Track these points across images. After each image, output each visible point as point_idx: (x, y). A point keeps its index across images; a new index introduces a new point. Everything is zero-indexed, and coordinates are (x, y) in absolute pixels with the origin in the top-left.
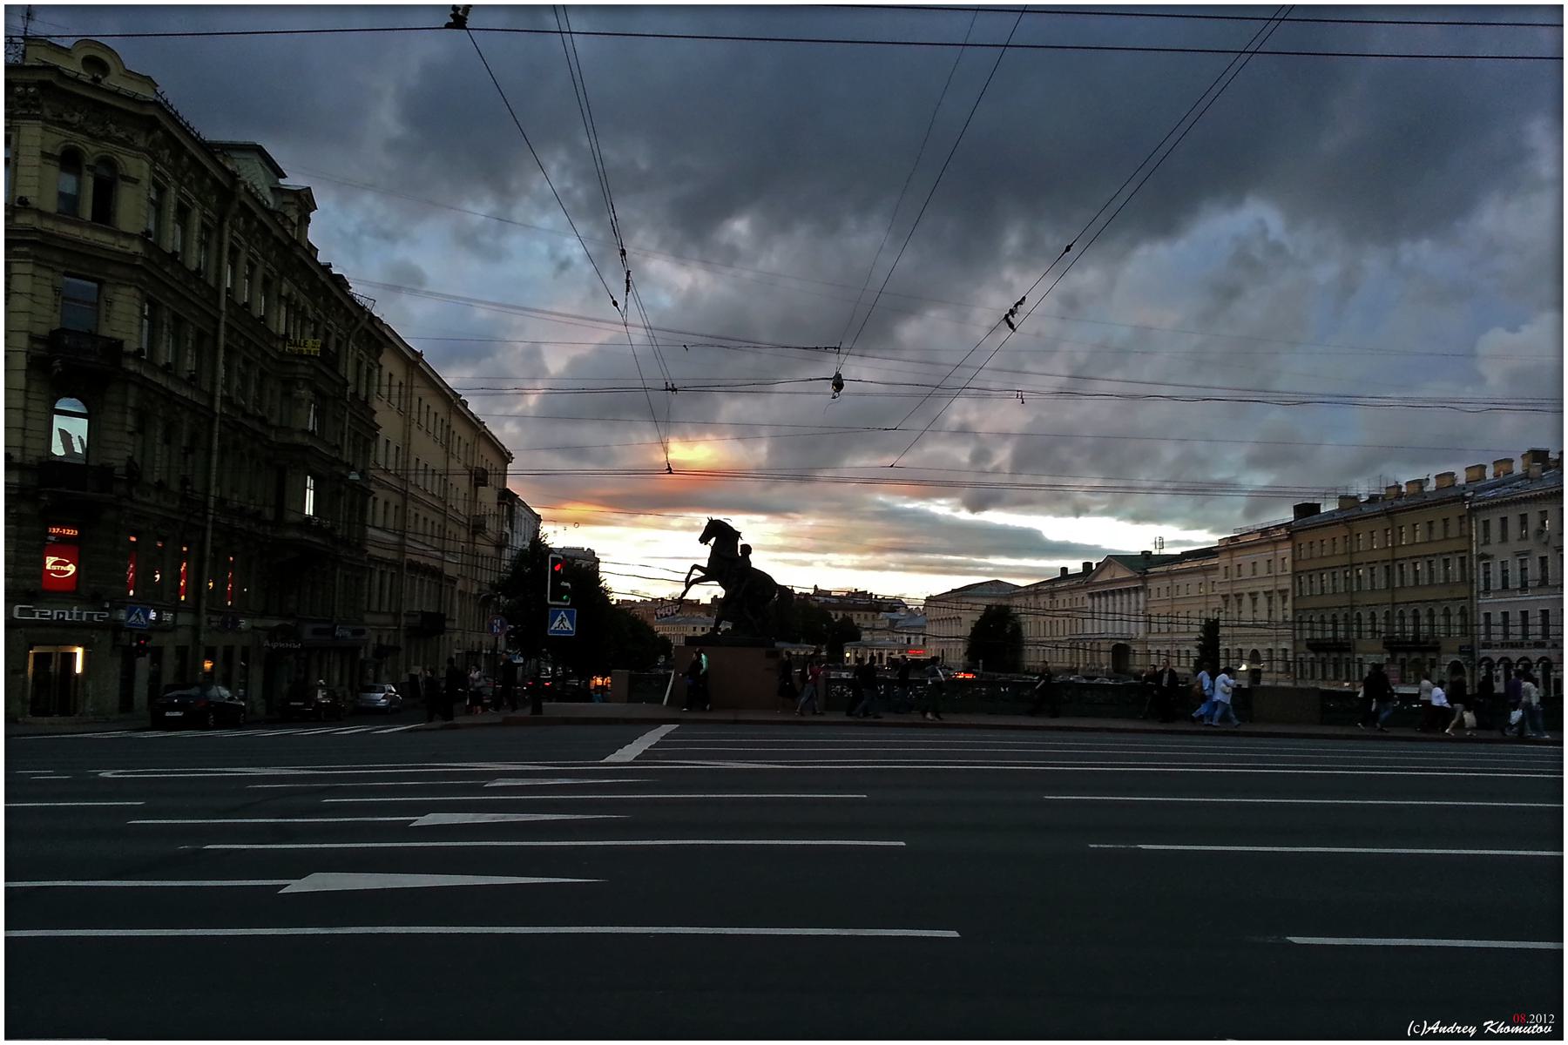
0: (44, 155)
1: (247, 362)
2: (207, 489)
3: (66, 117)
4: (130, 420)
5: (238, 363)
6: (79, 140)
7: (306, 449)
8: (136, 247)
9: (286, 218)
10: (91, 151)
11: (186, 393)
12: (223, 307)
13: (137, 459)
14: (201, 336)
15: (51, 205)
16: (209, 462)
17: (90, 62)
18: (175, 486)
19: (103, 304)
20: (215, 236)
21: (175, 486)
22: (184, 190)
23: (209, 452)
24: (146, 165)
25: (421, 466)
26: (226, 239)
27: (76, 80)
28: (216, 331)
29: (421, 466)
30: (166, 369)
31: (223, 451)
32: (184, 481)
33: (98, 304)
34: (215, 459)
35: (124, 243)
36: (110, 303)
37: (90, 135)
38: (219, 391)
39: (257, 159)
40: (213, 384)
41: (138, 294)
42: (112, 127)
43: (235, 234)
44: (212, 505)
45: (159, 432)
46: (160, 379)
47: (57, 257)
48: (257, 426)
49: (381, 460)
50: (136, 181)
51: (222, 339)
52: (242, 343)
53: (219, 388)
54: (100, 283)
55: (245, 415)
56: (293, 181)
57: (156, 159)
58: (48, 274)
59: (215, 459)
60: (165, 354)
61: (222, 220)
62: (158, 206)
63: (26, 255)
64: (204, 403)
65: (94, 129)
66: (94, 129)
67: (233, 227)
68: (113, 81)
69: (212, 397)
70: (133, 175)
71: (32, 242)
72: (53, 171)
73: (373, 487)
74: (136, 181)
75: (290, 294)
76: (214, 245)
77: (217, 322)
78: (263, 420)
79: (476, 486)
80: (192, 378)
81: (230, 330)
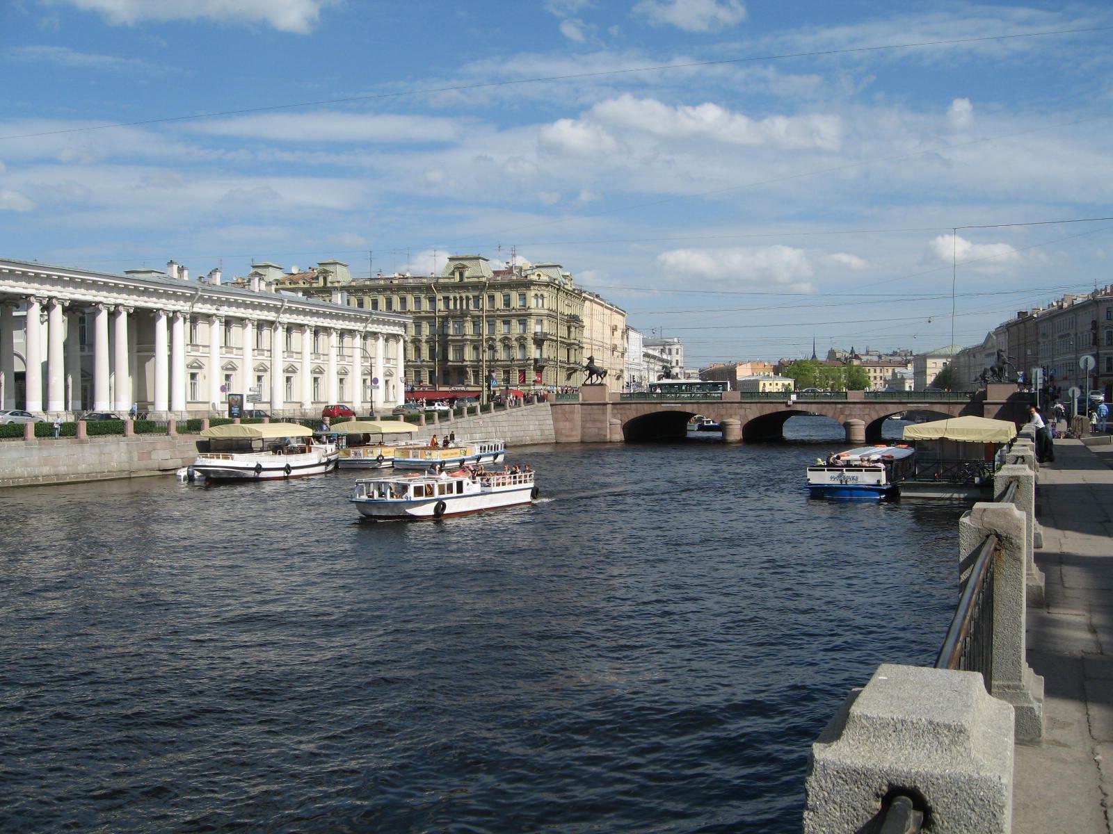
10: (539, 294)
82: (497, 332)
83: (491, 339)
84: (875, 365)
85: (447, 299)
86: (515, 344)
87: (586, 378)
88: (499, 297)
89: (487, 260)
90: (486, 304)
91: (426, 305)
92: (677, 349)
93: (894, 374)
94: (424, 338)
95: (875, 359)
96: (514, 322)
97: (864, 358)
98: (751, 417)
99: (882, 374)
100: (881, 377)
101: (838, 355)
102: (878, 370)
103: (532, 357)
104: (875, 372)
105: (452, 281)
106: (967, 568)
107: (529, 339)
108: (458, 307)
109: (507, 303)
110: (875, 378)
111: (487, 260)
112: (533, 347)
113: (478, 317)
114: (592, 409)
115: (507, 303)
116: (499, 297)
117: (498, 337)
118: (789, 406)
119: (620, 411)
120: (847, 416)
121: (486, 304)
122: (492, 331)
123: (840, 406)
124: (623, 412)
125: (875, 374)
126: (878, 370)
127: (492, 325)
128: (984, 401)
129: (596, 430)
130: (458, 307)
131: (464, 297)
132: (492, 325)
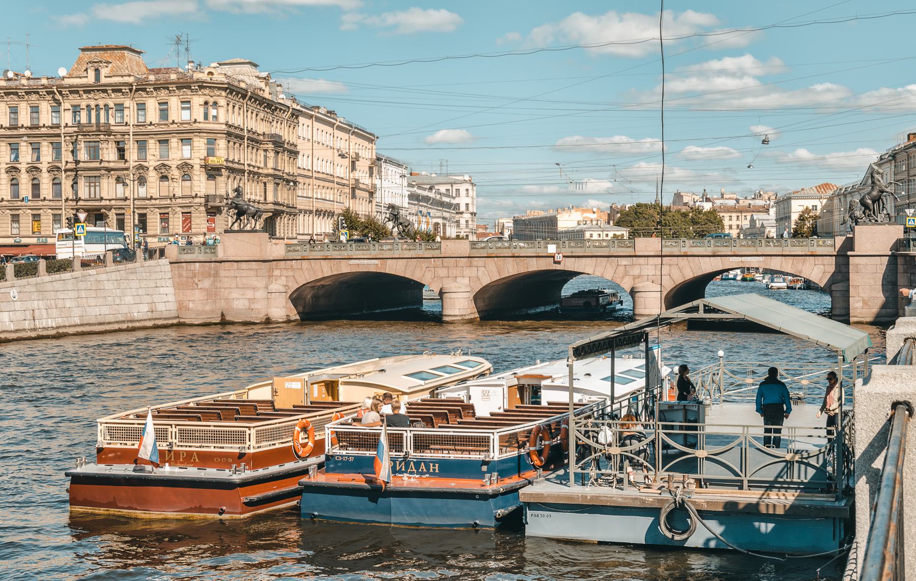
5: (250, 148)
10: (211, 100)
55: (254, 167)
66: (211, 94)
82: (149, 157)
83: (141, 167)
84: (729, 210)
85: (76, 110)
86: (176, 173)
87: (230, 220)
88: (152, 105)
89: (139, 53)
90: (131, 115)
91: (46, 117)
92: (467, 190)
93: (753, 221)
94: (44, 166)
95: (732, 203)
96: (174, 142)
97: (718, 202)
98: (486, 281)
99: (739, 223)
100: (738, 226)
101: (685, 200)
102: (734, 218)
103: (202, 194)
104: (730, 220)
105: (84, 81)
106: (878, 454)
107: (197, 167)
108: (93, 121)
109: (164, 113)
110: (731, 227)
111: (139, 53)
112: (203, 177)
113: (124, 134)
114: (210, 268)
115: (164, 113)
116: (152, 105)
117: (173, 164)
118: (559, 263)
119: (285, 273)
120: (635, 278)
121: (131, 115)
122: (165, 155)
123: (624, 261)
124: (290, 273)
125: (730, 223)
126: (734, 218)
127: (142, 146)
128: (849, 253)
129: (246, 303)
130: (93, 121)
131: (102, 106)
132: (142, 146)
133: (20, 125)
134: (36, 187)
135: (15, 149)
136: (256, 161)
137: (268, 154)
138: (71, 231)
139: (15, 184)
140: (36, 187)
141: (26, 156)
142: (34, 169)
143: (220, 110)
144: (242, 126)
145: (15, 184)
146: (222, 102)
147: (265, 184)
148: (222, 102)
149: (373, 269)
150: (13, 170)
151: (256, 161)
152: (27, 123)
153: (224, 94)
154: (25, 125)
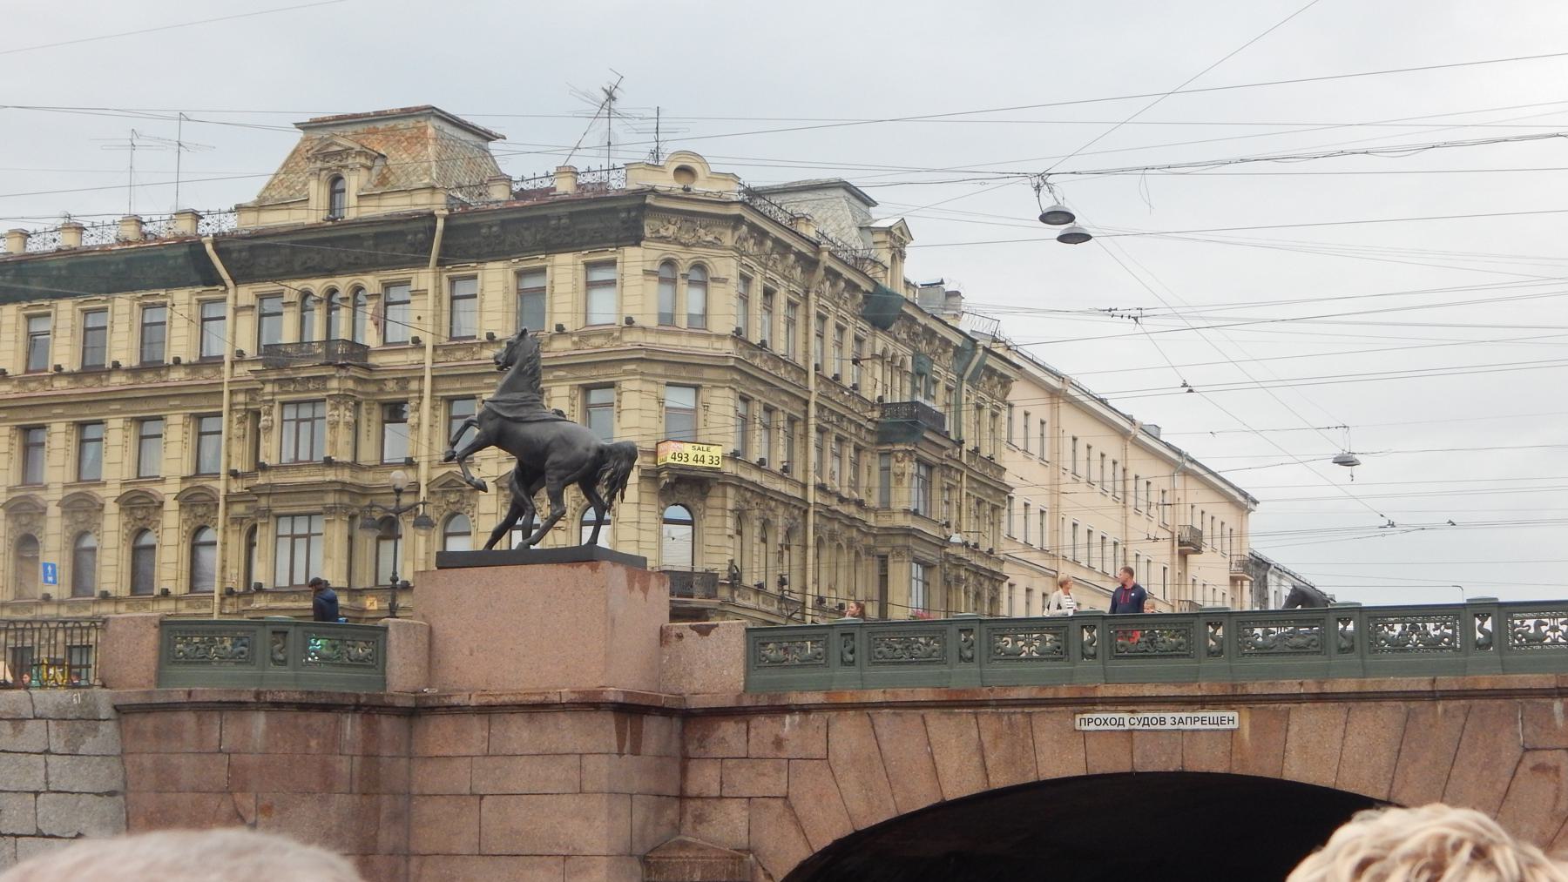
0: (647, 273)
1: (840, 440)
2: (805, 587)
3: (663, 233)
4: (730, 522)
5: (830, 444)
6: (673, 250)
7: (908, 532)
8: (728, 347)
9: (875, 263)
10: (685, 258)
11: (780, 486)
12: (812, 386)
13: (737, 563)
14: (792, 420)
15: (652, 322)
16: (805, 559)
17: (684, 171)
18: (772, 587)
19: (701, 412)
20: (801, 309)
21: (772, 587)
22: (769, 274)
23: (805, 547)
24: (733, 262)
25: (1096, 539)
26: (813, 310)
27: (667, 196)
28: (806, 413)
29: (1096, 539)
30: (760, 465)
31: (819, 543)
32: (782, 582)
33: (695, 410)
34: (811, 552)
35: (718, 345)
36: (706, 407)
37: (684, 245)
38: (812, 479)
39: (842, 192)
40: (806, 471)
41: (731, 394)
42: (702, 232)
43: (822, 301)
44: (809, 604)
45: (757, 531)
46: (755, 476)
47: (660, 369)
48: (851, 510)
49: (1018, 533)
50: (725, 281)
51: (812, 421)
52: (834, 419)
53: (811, 474)
54: (697, 388)
55: (842, 500)
56: (883, 217)
57: (742, 253)
58: (653, 387)
59: (811, 552)
60: (756, 453)
61: (807, 292)
62: (744, 299)
63: (633, 373)
64: (798, 493)
65: (686, 238)
66: (686, 238)
67: (818, 294)
68: (699, 187)
69: (805, 486)
70: (722, 275)
71: (642, 359)
72: (653, 285)
73: (1006, 569)
74: (725, 281)
75: (885, 351)
76: (800, 320)
77: (807, 403)
78: (860, 504)
79: (1183, 556)
80: (785, 469)
81: (821, 408)
108: (317, 334)
133: (169, 360)
134: (141, 555)
135: (30, 440)
136: (855, 485)
137: (896, 467)
138: (76, 697)
139: (27, 544)
140: (141, 555)
141: (57, 465)
142: (82, 507)
143: (716, 292)
144: (800, 361)
145: (27, 544)
146: (725, 266)
147: (884, 560)
148: (725, 266)
149: (1209, 760)
150: (24, 509)
151: (855, 485)
152: (188, 354)
153: (729, 239)
154: (66, 369)
